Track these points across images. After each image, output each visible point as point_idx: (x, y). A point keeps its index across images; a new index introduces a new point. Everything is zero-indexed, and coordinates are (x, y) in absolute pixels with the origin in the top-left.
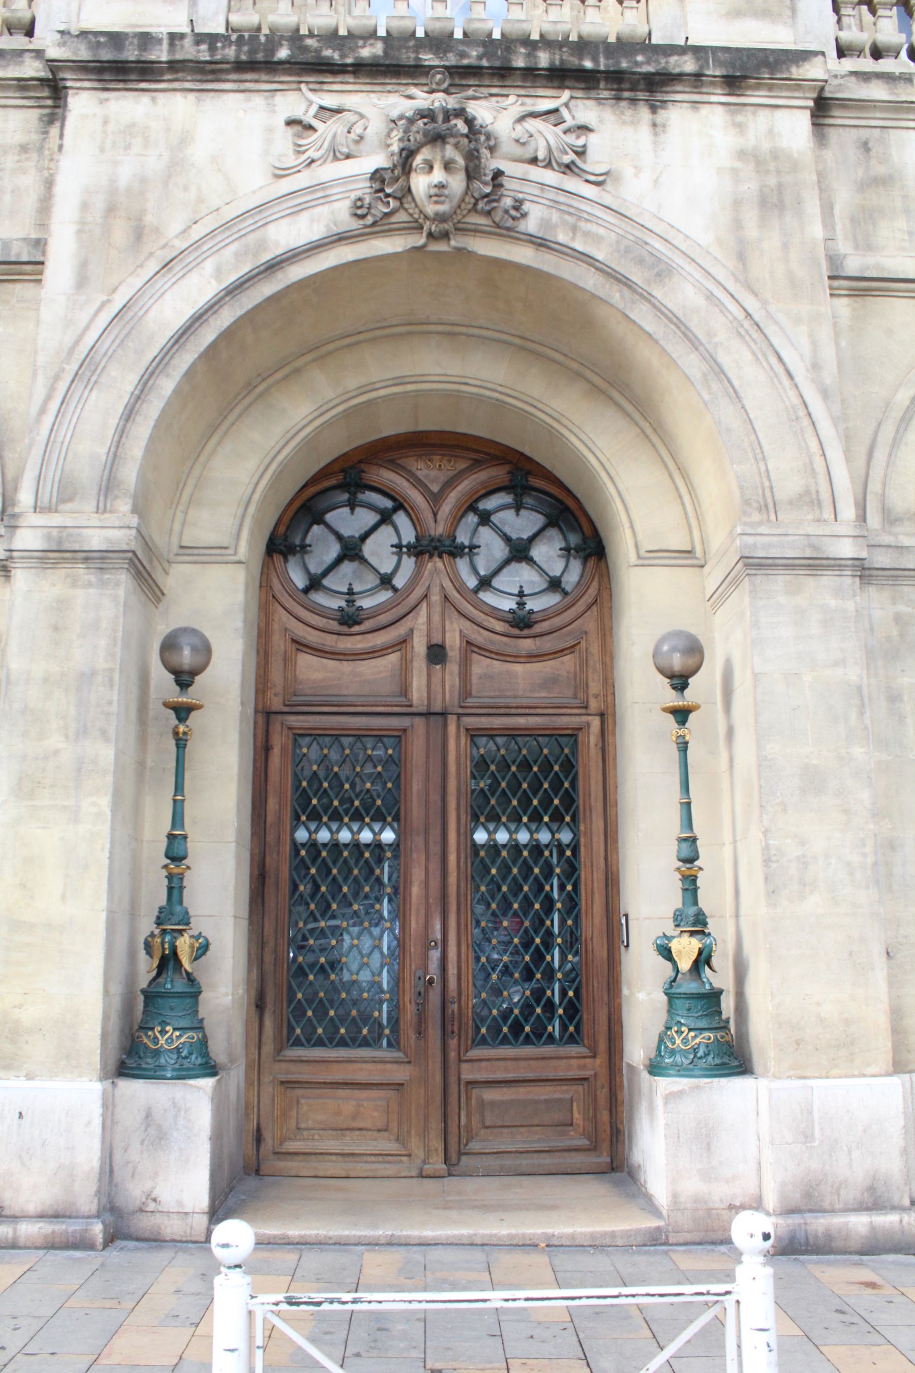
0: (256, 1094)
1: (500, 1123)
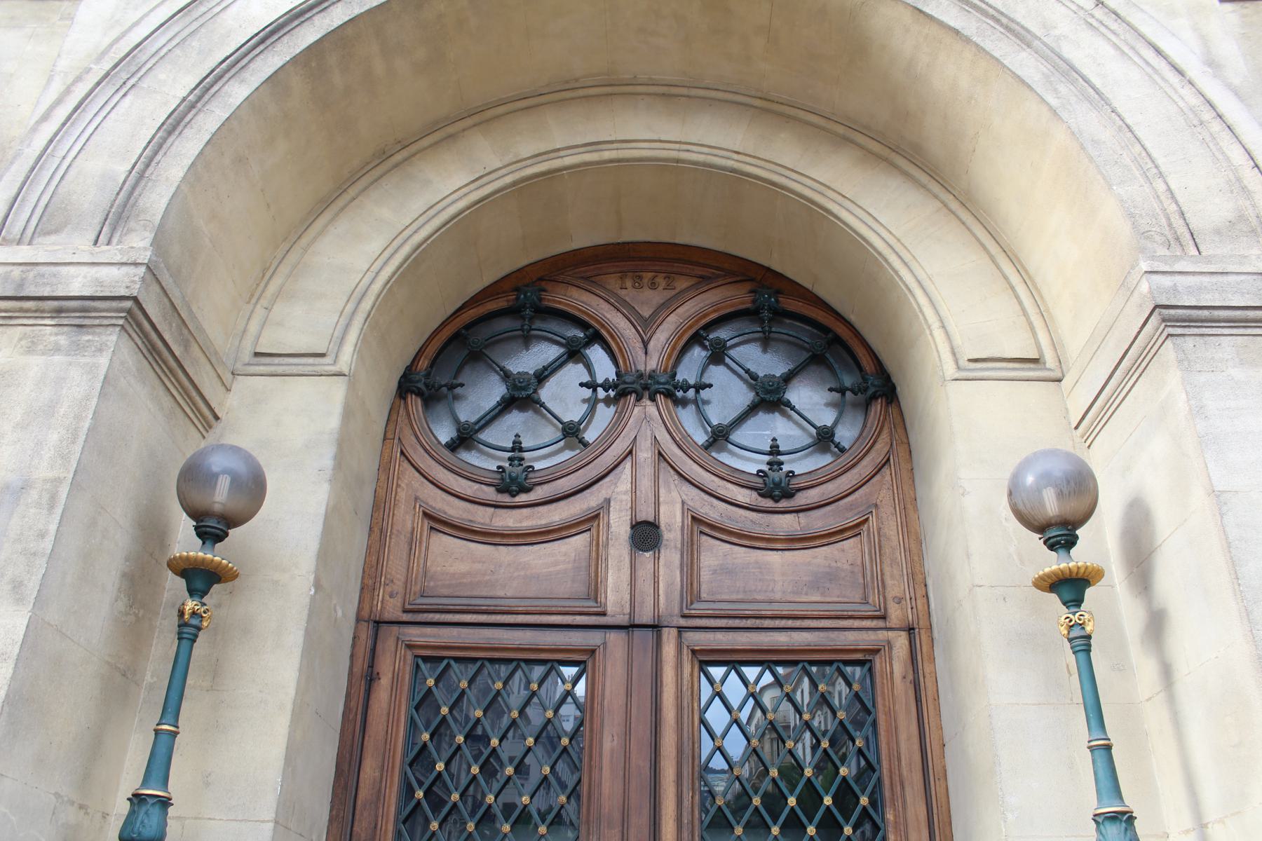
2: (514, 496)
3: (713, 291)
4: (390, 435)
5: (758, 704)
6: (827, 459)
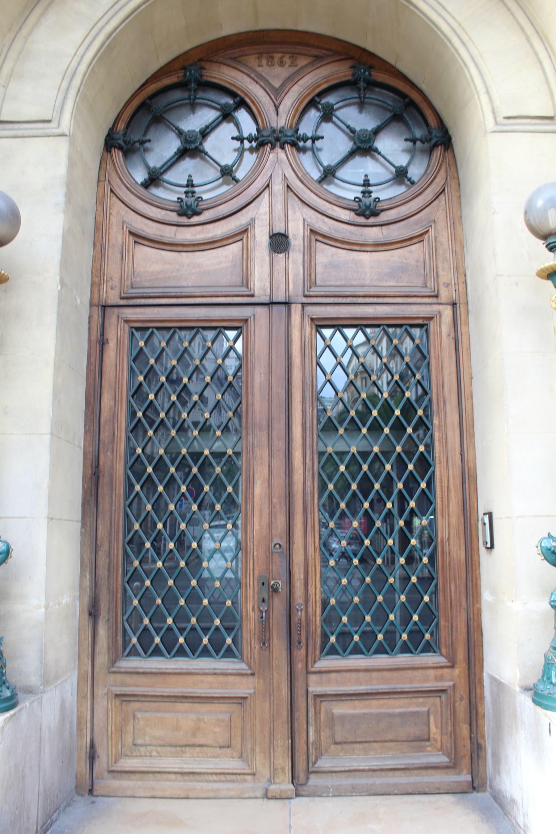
0: (89, 708)
1: (351, 739)
2: (189, 218)
3: (325, 67)
4: (102, 179)
5: (354, 353)
6: (403, 189)
